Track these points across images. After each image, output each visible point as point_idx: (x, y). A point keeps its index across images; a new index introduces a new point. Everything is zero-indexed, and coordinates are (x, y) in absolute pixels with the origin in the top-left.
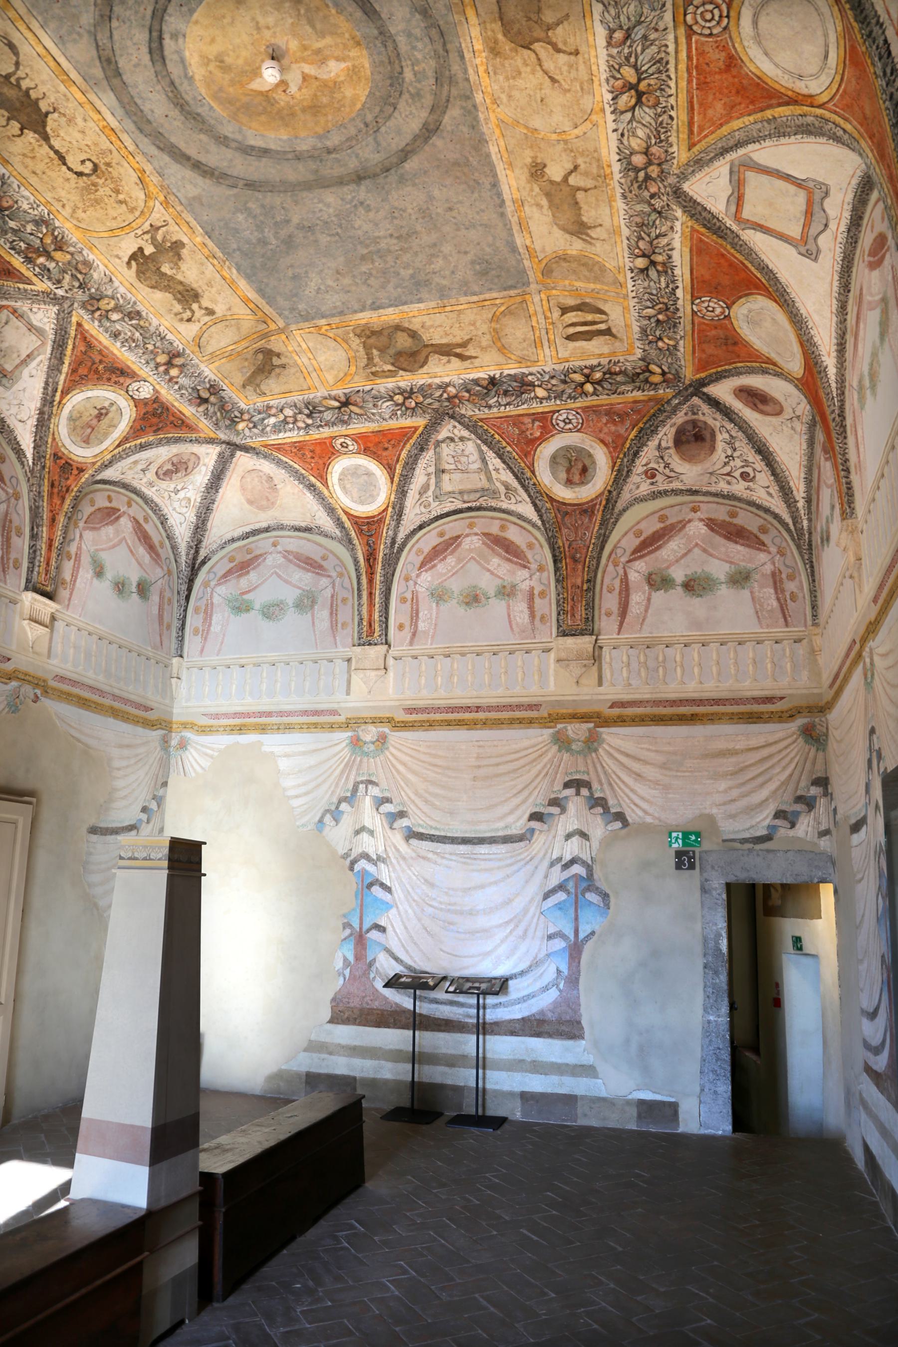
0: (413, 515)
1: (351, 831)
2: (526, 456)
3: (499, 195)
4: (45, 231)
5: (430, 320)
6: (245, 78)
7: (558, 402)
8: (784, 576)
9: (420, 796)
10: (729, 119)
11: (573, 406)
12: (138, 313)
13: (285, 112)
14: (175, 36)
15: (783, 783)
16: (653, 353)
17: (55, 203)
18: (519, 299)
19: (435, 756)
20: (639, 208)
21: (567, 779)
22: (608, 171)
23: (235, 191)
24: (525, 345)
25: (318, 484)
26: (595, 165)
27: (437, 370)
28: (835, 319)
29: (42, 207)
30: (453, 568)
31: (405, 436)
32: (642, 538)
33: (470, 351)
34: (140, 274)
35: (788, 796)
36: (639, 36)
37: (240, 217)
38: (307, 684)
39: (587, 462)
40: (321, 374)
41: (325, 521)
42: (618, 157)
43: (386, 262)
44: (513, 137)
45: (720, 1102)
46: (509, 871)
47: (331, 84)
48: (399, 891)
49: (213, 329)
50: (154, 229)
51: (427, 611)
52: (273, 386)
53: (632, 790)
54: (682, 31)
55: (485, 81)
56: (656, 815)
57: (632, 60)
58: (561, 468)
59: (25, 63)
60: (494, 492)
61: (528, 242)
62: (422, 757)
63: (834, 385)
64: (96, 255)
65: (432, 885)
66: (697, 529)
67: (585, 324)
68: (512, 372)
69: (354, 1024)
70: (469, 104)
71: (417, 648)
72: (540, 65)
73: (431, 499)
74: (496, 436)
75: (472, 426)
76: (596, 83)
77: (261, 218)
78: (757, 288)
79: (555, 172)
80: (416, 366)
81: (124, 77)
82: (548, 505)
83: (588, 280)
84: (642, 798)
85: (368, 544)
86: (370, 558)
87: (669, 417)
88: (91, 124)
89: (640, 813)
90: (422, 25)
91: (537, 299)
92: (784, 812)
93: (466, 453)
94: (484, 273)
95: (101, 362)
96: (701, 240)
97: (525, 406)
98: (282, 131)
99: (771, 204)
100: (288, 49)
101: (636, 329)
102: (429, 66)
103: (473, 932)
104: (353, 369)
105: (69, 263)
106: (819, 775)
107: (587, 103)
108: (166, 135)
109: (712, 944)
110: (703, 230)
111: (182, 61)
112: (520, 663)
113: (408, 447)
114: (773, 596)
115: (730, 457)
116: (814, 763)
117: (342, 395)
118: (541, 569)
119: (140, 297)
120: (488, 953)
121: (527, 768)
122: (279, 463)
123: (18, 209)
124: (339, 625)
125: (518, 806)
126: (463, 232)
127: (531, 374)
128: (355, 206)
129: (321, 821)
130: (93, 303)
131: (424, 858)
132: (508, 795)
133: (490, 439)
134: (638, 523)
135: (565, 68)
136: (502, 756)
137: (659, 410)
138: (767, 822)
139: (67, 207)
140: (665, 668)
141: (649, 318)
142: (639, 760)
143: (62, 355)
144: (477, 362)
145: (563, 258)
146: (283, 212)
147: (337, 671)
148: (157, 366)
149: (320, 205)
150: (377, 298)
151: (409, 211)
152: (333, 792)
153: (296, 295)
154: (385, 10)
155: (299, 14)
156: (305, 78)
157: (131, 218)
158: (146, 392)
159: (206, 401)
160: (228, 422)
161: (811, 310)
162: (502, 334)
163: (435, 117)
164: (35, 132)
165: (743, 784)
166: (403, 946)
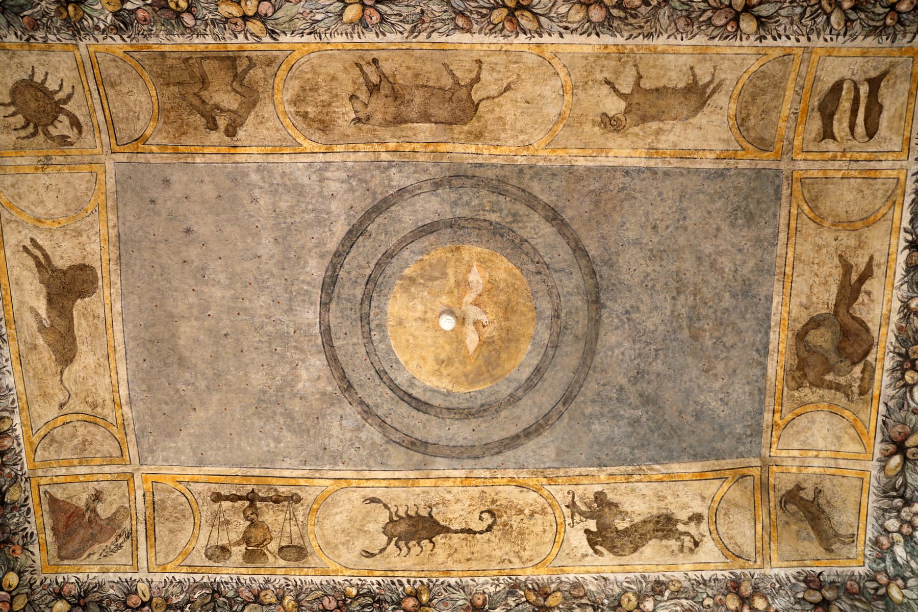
3: (639, 170)
4: (522, 593)
6: (463, 351)
13: (503, 335)
18: (797, 186)
20: (664, 21)
23: (566, 415)
24: (867, 192)
27: (878, 312)
29: (501, 578)
33: (860, 262)
42: (594, 36)
44: (567, 139)
49: (722, 530)
50: (572, 506)
55: (504, 150)
57: (484, 11)
59: (388, 501)
64: (572, 572)
67: (854, 112)
68: (907, 216)
72: (493, 98)
77: (606, 410)
79: (614, 106)
80: (864, 336)
81: (430, 441)
88: (455, 490)
91: (803, 165)
98: (522, 346)
101: (871, 41)
102: (487, 197)
104: (847, 413)
105: (565, 598)
107: (531, 59)
108: (490, 441)
111: (433, 391)
117: (884, 446)
123: (490, 596)
128: (628, 319)
139: (513, 559)
144: (879, 258)
145: (741, 122)
146: (608, 388)
149: (616, 351)
150: (753, 345)
151: (649, 270)
153: (722, 428)
155: (424, 285)
162: (843, 217)
164: (439, 534)
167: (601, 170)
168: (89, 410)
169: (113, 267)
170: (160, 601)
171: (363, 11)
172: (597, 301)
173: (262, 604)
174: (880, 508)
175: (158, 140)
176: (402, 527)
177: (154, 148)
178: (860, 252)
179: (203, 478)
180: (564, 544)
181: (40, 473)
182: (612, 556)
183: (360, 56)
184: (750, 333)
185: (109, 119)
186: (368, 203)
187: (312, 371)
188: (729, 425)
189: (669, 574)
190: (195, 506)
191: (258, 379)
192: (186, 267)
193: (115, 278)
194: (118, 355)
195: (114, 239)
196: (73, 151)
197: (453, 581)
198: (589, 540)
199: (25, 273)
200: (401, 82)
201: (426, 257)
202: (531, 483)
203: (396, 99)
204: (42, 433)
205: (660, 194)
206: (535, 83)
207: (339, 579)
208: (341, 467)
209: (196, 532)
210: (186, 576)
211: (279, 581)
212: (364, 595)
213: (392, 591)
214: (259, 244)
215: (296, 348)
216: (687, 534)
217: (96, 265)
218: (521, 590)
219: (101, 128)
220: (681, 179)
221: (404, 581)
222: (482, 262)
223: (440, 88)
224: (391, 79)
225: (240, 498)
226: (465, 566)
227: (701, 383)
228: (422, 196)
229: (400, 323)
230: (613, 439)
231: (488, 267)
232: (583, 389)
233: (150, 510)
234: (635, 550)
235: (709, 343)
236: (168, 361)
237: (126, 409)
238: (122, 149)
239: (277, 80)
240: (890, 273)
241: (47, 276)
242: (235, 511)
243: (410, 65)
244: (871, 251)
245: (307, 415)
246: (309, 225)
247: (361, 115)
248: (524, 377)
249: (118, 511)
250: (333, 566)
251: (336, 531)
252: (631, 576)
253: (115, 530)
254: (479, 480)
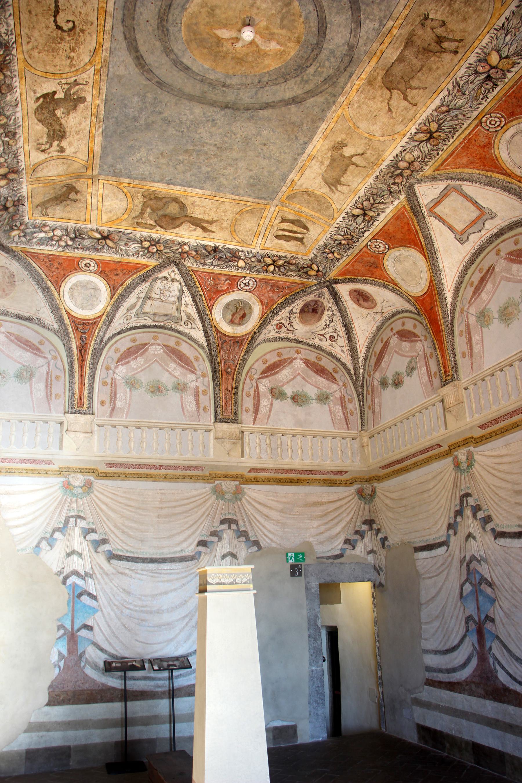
0: (118, 323)
1: (63, 554)
2: (210, 300)
5: (199, 201)
7: (248, 272)
8: (346, 400)
9: (119, 528)
10: (466, 166)
11: (256, 276)
13: (222, 54)
15: (348, 523)
18: (263, 206)
19: (129, 499)
20: (380, 185)
21: (222, 518)
23: (148, 82)
27: (184, 233)
28: (458, 274)
29: (14, 37)
30: (142, 365)
31: (136, 269)
32: (267, 365)
33: (213, 228)
35: (351, 531)
38: (26, 438)
40: (99, 213)
42: (392, 159)
43: (198, 158)
44: (341, 125)
45: (320, 720)
46: (184, 581)
47: (262, 53)
48: (103, 599)
51: (123, 394)
53: (263, 526)
55: (353, 93)
56: (278, 542)
57: (441, 122)
60: (178, 319)
62: (119, 499)
63: (449, 308)
65: (129, 593)
66: (298, 364)
67: (290, 231)
69: (68, 704)
71: (115, 420)
72: (389, 101)
73: (133, 315)
74: (197, 283)
75: (185, 274)
77: (148, 105)
79: (348, 152)
80: (171, 226)
82: (215, 334)
83: (313, 209)
84: (270, 531)
86: (82, 349)
87: (305, 296)
89: (269, 541)
90: (344, 52)
91: (272, 209)
92: (349, 540)
93: (171, 289)
96: (403, 213)
97: (227, 270)
101: (321, 243)
102: (326, 72)
103: (160, 626)
104: (126, 216)
106: (366, 518)
107: (399, 128)
108: (136, 32)
109: (312, 622)
112: (190, 438)
113: (134, 277)
114: (341, 411)
115: (328, 326)
116: (363, 511)
118: (203, 375)
120: (171, 640)
121: (196, 510)
122: (27, 267)
124: (53, 396)
125: (189, 536)
126: (261, 159)
129: (38, 546)
131: (122, 573)
132: (183, 529)
134: (265, 355)
136: (177, 501)
137: (303, 290)
138: (340, 547)
140: (281, 449)
142: (267, 507)
144: (212, 235)
147: (52, 430)
151: (239, 136)
152: (48, 524)
153: (121, 158)
154: (331, 36)
162: (238, 223)
163: (305, 96)
165: (327, 523)
166: (107, 640)
167: (314, 133)
171: (490, 65)
172: (227, 107)
174: (67, 228)
178: (218, 228)
180: (45, 79)
182: (35, 107)
183: (465, 46)
184: (183, 177)
188: (122, 162)
189: (22, 139)
198: (47, 94)
200: (433, 59)
201: (301, 20)
202: (97, 58)
203: (424, 49)
205: (285, 153)
206: (384, 124)
216: (51, 146)
218: (4, 52)
220: (289, 164)
222: (282, 53)
223: (413, 77)
224: (438, 54)
227: (154, 150)
228: (348, 35)
230: (125, 108)
231: (276, 55)
232: (166, 93)
234: (40, 121)
235: (181, 158)
240: (204, 239)
243: (439, 70)
244: (217, 232)
247: (428, 22)
252: (20, 120)
254: (103, 22)
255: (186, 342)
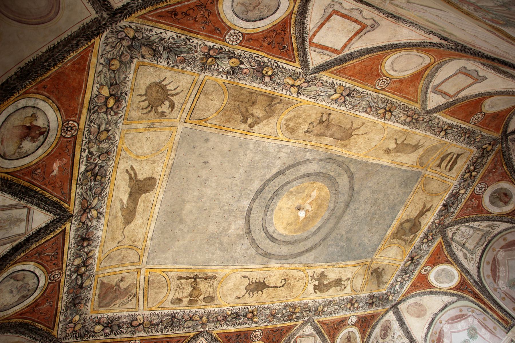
0: (472, 267)
3: (386, 166)
7: (471, 188)
11: (477, 183)
12: (330, 301)
14: (274, 232)
16: (479, 144)
17: (284, 299)
18: (424, 179)
22: (405, 130)
23: (322, 245)
24: (441, 186)
25: (432, 290)
26: (400, 133)
27: (426, 221)
30: (505, 270)
31: (440, 248)
33: (428, 206)
34: (321, 291)
36: (373, 104)
37: (330, 249)
39: (503, 191)
41: (449, 299)
49: (354, 282)
50: (312, 277)
52: (387, 277)
54: (381, 92)
55: (351, 153)
57: (378, 109)
58: (498, 202)
61: (407, 165)
68: (447, 196)
70: (353, 161)
73: (471, 256)
76: (376, 122)
78: (482, 100)
80: (419, 227)
82: (509, 217)
83: (435, 153)
85: (470, 292)
86: (475, 295)
91: (428, 173)
93: (464, 231)
94: (406, 185)
95: (334, 325)
97: (463, 200)
99: (455, 85)
100: (300, 204)
102: (335, 166)
107: (380, 127)
110: (447, 109)
111: (281, 234)
113: (445, 250)
119: (327, 297)
122: (413, 296)
124: (493, 330)
127: (453, 191)
130: (317, 312)
133: (465, 220)
135: (365, 129)
137: (503, 153)
141: (464, 139)
143: (322, 334)
144: (434, 206)
145: (421, 157)
148: (350, 309)
153: (365, 248)
156: (310, 204)
157: (305, 281)
158: (354, 319)
159: (373, 303)
160: (385, 301)
161: (505, 87)
167: (377, 164)
168: (131, 243)
169: (165, 178)
170: (147, 322)
173: (193, 321)
175: (213, 122)
176: (252, 287)
177: (209, 125)
179: (175, 270)
181: (100, 272)
185: (192, 108)
186: (292, 163)
187: (237, 226)
190: (168, 282)
191: (212, 228)
192: (199, 179)
193: (164, 184)
194: (153, 219)
195: (170, 165)
196: (165, 120)
197: (266, 306)
199: (124, 183)
204: (106, 255)
207: (225, 308)
208: (236, 264)
209: (168, 293)
210: (160, 312)
211: (201, 311)
212: (233, 314)
213: (244, 311)
214: (237, 172)
215: (234, 216)
217: (157, 178)
219: (185, 110)
221: (249, 307)
225: (190, 278)
226: (271, 300)
229: (280, 209)
233: (147, 284)
235: (374, 222)
236: (175, 220)
237: (149, 242)
238: (191, 122)
239: (287, 110)
241: (133, 184)
242: (187, 284)
245: (229, 244)
246: (263, 168)
248: (314, 230)
249: (130, 285)
250: (224, 303)
251: (228, 290)
253: (128, 293)
255: (507, 234)
